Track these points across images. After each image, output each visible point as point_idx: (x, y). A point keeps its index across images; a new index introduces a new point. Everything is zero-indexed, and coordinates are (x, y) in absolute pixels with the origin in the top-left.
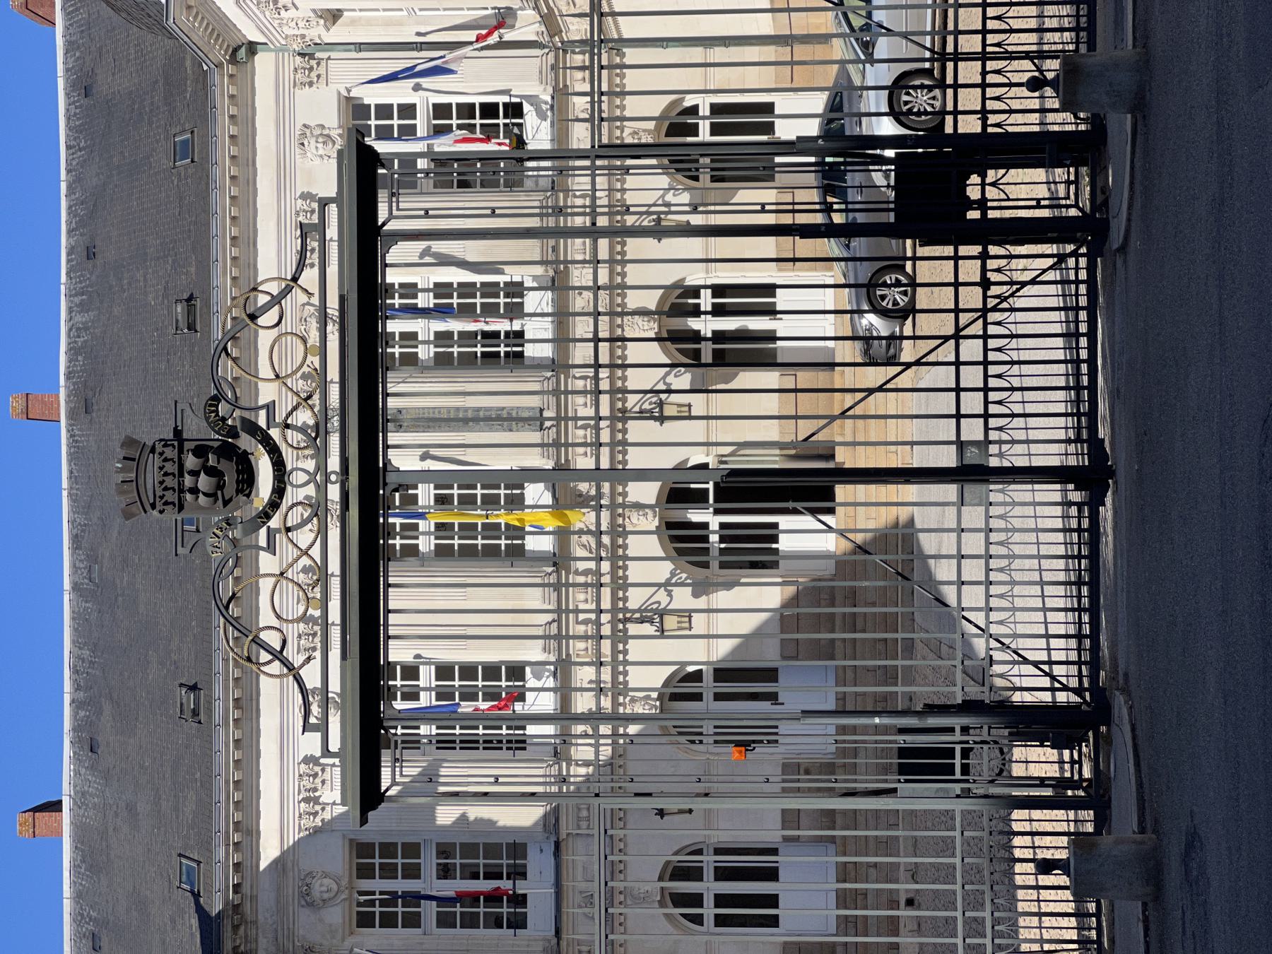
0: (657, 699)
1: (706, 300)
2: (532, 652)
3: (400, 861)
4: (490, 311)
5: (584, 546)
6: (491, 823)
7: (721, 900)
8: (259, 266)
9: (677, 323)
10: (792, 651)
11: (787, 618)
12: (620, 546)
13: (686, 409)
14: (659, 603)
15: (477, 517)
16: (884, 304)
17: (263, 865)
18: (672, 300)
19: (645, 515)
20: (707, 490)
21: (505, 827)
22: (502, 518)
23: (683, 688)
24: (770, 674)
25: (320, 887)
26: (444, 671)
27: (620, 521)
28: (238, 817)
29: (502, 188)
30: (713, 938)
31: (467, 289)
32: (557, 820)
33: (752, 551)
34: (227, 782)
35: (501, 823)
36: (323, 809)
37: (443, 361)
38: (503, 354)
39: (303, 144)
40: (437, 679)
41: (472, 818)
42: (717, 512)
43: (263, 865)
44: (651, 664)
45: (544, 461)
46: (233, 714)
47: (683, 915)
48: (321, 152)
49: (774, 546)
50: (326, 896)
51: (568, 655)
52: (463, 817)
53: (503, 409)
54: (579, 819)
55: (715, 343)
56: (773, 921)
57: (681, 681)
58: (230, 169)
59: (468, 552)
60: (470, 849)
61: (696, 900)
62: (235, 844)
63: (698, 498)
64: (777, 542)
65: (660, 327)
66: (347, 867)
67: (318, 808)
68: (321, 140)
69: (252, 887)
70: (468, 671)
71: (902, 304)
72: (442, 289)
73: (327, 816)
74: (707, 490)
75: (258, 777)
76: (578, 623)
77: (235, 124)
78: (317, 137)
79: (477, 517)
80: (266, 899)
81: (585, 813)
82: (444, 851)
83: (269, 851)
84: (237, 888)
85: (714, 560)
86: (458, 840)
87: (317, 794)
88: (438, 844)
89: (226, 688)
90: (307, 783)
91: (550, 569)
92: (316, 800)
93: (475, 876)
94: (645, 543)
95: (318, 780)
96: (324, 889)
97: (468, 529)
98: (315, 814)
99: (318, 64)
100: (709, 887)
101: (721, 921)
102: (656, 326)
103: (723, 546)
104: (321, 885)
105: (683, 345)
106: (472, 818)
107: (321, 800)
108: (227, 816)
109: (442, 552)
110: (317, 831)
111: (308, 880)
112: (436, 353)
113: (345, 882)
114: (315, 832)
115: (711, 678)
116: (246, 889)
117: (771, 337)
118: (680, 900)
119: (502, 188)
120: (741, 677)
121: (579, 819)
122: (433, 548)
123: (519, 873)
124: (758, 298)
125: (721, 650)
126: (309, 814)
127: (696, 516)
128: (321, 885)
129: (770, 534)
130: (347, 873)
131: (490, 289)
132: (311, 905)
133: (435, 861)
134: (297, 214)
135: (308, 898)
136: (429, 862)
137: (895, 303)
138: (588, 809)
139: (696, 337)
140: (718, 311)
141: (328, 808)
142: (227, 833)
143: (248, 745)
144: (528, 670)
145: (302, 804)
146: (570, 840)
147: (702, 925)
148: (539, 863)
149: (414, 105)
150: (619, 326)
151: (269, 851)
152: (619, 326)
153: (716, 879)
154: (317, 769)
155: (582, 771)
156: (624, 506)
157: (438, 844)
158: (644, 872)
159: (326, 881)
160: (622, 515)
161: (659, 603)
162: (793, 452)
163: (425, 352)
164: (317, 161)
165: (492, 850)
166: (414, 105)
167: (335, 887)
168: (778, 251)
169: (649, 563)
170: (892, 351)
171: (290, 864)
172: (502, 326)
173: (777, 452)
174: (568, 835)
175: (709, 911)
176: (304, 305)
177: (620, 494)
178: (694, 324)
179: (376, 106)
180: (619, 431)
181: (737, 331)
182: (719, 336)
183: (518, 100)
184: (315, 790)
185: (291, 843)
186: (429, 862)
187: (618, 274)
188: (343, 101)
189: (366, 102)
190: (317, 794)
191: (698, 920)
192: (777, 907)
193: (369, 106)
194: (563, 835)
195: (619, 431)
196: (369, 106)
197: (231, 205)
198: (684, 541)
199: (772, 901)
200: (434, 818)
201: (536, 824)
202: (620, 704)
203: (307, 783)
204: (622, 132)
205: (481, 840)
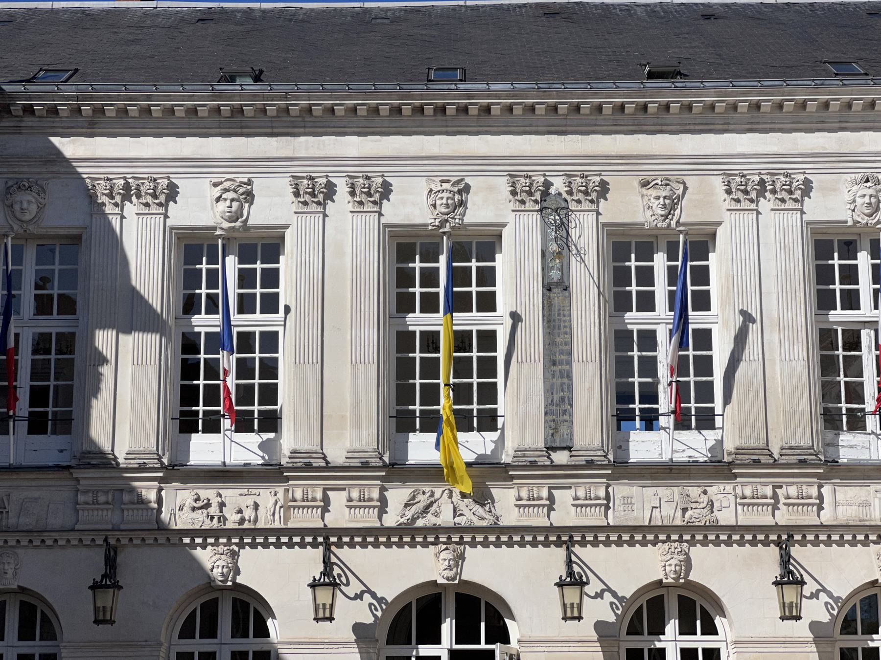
0: (234, 583)
2: (290, 440)
3: (258, 291)
5: (414, 498)
6: (95, 391)
8: (726, 135)
9: (672, 606)
13: (576, 614)
14: (348, 584)
15: (445, 377)
17: (56, 140)
19: (450, 568)
21: (89, 407)
22: (445, 405)
25: (28, 202)
26: (270, 341)
28: (110, 111)
29: (823, 405)
31: (705, 366)
32: (94, 466)
34: (149, 98)
35: (94, 402)
36: (116, 205)
37: (622, 338)
38: (630, 406)
39: (867, 181)
40: (239, 333)
41: (103, 370)
43: (56, 140)
45: (511, 452)
46: (225, 105)
47: (195, 611)
48: (859, 201)
50: (17, 207)
51: (288, 479)
52: (104, 360)
53: (571, 405)
54: (96, 492)
57: (256, 612)
58: (609, 103)
59: (404, 369)
60: (66, 370)
61: (210, 631)
62: (79, 106)
65: (668, 586)
66: (50, 232)
67: (118, 199)
68: (873, 200)
69: (31, 127)
70: (270, 369)
72: (704, 338)
73: (109, 209)
75: (359, 134)
77: (865, 107)
78: (876, 197)
79: (445, 377)
80: (18, 144)
81: (102, 498)
82: (67, 343)
83: (70, 147)
84: (29, 110)
86: (77, 356)
87: (134, 198)
88: (73, 334)
89: (254, 97)
90: (147, 187)
91: (386, 459)
92: (127, 197)
94: (425, 566)
95: (149, 199)
96: (25, 206)
97: (431, 368)
98: (111, 196)
99: (374, 202)
104: (29, 202)
107: (127, 203)
108: (110, 98)
109: (405, 340)
110: (92, 197)
111: (35, 188)
112: (632, 331)
113: (33, 229)
114: (91, 197)
115: (258, 648)
116: (28, 121)
118: (210, 611)
119: (823, 405)
121: (96, 492)
122: (411, 328)
123: (682, 422)
126: (112, 189)
127: (448, 628)
128: (29, 202)
130: (43, 232)
131: (705, 392)
132: (8, 190)
133: (54, 331)
134: (787, 175)
135: (15, 187)
136: (54, 324)
138: (107, 503)
139: (658, 630)
141: (117, 210)
142: (92, 98)
143: (528, 122)
144: (272, 435)
145: (122, 182)
146: (73, 483)
148: (47, 448)
149: (494, 310)
150: (669, 537)
151: (70, 147)
152: (669, 537)
154: (162, 198)
155: (152, 496)
156: (328, 546)
157: (73, 334)
158: (484, 568)
159: (34, 208)
160: (449, 542)
161: (348, 584)
164: (848, 197)
165: (66, 396)
166: (494, 310)
167: (27, 217)
171: (55, 169)
172: (665, 403)
176: (684, 183)
179: (707, 267)
180: (547, 537)
183: (499, 426)
184: (139, 196)
185: (80, 170)
186: (54, 324)
187: (730, 537)
188: (710, 228)
189: (711, 255)
190: (134, 198)
193: (494, 261)
194: (77, 474)
196: (707, 260)
197: (637, 103)
200: (103, 327)
201: (92, 442)
203: (147, 187)
204: (456, 543)
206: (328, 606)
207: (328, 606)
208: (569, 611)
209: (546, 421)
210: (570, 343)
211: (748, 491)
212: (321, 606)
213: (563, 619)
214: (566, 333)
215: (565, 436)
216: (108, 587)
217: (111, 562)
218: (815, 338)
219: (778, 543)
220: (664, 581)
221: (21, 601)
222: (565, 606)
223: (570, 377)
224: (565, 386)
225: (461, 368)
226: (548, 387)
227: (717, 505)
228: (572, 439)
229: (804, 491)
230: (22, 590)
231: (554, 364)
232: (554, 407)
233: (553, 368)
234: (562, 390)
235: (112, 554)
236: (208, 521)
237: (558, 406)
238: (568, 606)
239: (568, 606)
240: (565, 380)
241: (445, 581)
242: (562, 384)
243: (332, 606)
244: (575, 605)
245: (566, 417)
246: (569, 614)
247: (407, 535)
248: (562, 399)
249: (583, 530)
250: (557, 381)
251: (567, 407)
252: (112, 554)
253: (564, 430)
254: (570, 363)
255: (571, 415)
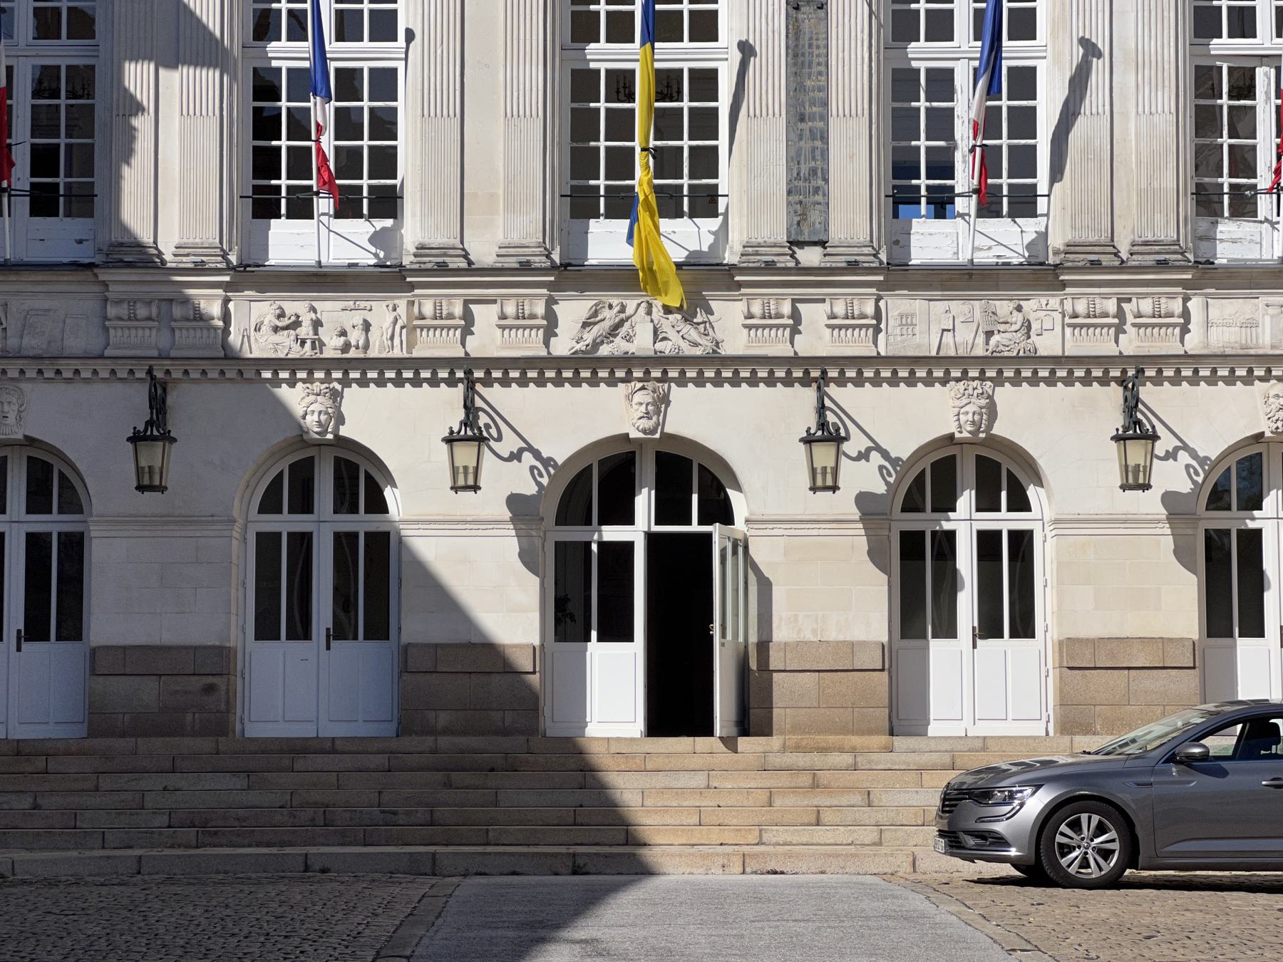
0: (337, 437)
1: (1004, 521)
2: (417, 228)
4: (989, 163)
5: (596, 314)
6: (127, 154)
7: (302, 543)
9: (967, 471)
10: (413, 664)
11: (486, 657)
12: (594, 373)
13: (829, 482)
14: (499, 439)
15: (642, 137)
16: (1063, 828)
18: (1006, 464)
19: (647, 416)
20: (689, 523)
21: (119, 177)
22: (642, 179)
23: (360, 478)
24: (379, 629)
26: (385, 82)
27: (638, 374)
29: (1196, 180)
30: (237, 528)
31: (1024, 122)
32: (130, 265)
33: (584, 600)
35: (126, 171)
37: (903, 82)
38: (912, 182)
40: (338, 70)
41: (137, 122)
42: (651, 538)
44: (399, 427)
45: (738, 249)
47: (281, 473)
49: (594, 634)
51: (412, 286)
53: (826, 181)
54: (133, 303)
55: (948, 540)
56: (266, 629)
57: (61, 474)
59: (583, 125)
60: (82, 121)
61: (304, 503)
63: (670, 509)
64: (600, 639)
65: (962, 443)
70: (385, 125)
71: (1064, 862)
72: (1025, 81)
74: (689, 523)
76: (466, 303)
79: (642, 137)
82: (82, 81)
85: (574, 534)
91: (556, 257)
93: (37, 128)
94: (613, 413)
97: (621, 125)
100: (324, 523)
101: (267, 543)
102: (966, 435)
103: (594, 547)
105: (933, 478)
106: (137, 122)
109: (583, 82)
112: (918, 71)
115: (372, 528)
117: (947, 629)
118: (302, 477)
120: (375, 574)
121: (133, 303)
122: (593, 65)
124: (1010, 613)
125: (429, 547)
127: (644, 503)
129: (617, 630)
131: (1024, 161)
137: (1066, 849)
140: (988, 541)
144: (388, 223)
146: (97, 288)
147: (1029, 510)
150: (965, 372)
152: (965, 372)
153: (338, 537)
155: (215, 309)
158: (699, 416)
160: (647, 377)
161: (499, 439)
162: (753, 665)
163: (923, 53)
165: (84, 160)
168: (779, 644)
169: (570, 422)
170: (971, 841)
173: (753, 639)
174: (105, 284)
175: (286, 523)
177: (683, 373)
178: (966, 501)
180: (789, 373)
181: (954, 571)
182: (946, 542)
187: (1053, 372)
191: (270, 504)
192: (1011, 636)
194: (104, 275)
195: (789, 373)
198: (603, 481)
199: (300, 629)
201: (125, 230)
202: (328, 373)
205: (98, 140)
206: (471, 470)
207: (471, 470)
208: (819, 478)
209: (789, 203)
210: (825, 89)
211: (1081, 307)
212: (461, 470)
213: (811, 489)
214: (820, 73)
215: (817, 226)
216: (154, 439)
217: (158, 403)
218: (1188, 81)
219: (1122, 382)
220: (957, 435)
221: (978, 457)
222: (813, 471)
223: (824, 138)
224: (818, 152)
225: (666, 124)
226: (793, 153)
227: (1035, 326)
228: (826, 230)
229: (1163, 306)
230: (30, 441)
231: (802, 119)
232: (801, 183)
233: (801, 126)
234: (814, 158)
235: (159, 391)
236: (297, 347)
237: (807, 182)
238: (819, 471)
239: (819, 471)
240: (818, 143)
241: (641, 435)
242: (814, 149)
243: (477, 469)
244: (829, 470)
245: (819, 198)
246: (819, 483)
247: (586, 367)
248: (813, 172)
249: (842, 362)
250: (806, 145)
251: (820, 183)
252: (159, 391)
253: (815, 216)
254: (824, 118)
255: (826, 195)
